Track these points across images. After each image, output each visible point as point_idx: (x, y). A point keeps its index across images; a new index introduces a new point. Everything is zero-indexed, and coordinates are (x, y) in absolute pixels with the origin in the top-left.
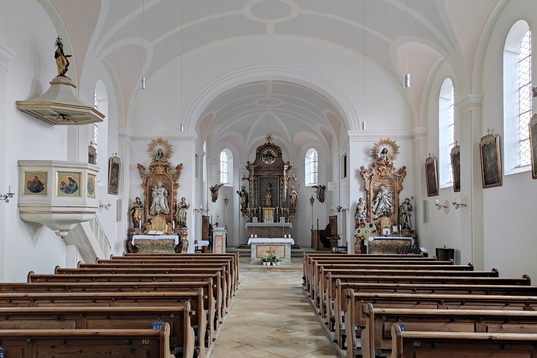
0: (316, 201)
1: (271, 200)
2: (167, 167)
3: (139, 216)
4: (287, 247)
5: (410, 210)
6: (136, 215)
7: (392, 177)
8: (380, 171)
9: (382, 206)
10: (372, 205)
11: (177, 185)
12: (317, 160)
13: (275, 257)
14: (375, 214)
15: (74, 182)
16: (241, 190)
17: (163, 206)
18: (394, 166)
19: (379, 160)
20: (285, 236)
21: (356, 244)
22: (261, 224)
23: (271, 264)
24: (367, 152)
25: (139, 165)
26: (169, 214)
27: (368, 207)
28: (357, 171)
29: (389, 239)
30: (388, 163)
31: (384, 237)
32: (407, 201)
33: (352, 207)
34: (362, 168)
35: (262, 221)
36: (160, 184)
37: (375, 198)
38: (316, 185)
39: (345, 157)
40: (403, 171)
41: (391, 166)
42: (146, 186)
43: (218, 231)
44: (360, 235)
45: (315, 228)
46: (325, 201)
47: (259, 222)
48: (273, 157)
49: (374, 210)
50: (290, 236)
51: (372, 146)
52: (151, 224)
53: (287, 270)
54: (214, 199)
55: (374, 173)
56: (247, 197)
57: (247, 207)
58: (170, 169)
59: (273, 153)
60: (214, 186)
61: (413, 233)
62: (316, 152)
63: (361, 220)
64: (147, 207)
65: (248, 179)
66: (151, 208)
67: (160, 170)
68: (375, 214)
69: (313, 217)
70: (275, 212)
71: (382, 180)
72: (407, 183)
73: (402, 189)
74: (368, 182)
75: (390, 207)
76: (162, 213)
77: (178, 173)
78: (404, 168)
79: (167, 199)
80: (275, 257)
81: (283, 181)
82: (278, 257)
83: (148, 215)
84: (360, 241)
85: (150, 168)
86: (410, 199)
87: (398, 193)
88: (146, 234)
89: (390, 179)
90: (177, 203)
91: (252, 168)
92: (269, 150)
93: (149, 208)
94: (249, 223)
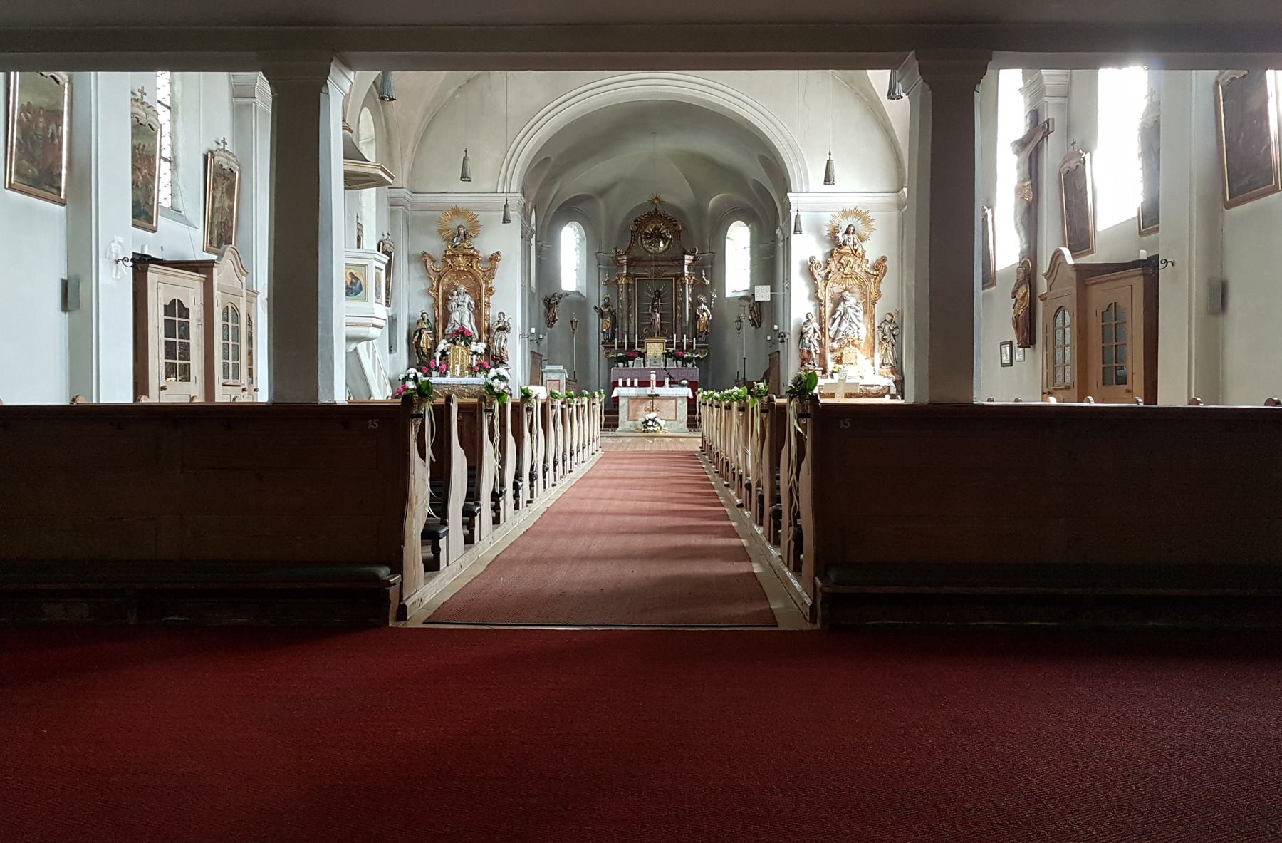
7: (863, 275)
10: (828, 323)
11: (490, 290)
34: (812, 259)
36: (463, 288)
37: (834, 313)
57: (613, 337)
63: (809, 352)
77: (493, 269)
78: (884, 259)
81: (683, 285)
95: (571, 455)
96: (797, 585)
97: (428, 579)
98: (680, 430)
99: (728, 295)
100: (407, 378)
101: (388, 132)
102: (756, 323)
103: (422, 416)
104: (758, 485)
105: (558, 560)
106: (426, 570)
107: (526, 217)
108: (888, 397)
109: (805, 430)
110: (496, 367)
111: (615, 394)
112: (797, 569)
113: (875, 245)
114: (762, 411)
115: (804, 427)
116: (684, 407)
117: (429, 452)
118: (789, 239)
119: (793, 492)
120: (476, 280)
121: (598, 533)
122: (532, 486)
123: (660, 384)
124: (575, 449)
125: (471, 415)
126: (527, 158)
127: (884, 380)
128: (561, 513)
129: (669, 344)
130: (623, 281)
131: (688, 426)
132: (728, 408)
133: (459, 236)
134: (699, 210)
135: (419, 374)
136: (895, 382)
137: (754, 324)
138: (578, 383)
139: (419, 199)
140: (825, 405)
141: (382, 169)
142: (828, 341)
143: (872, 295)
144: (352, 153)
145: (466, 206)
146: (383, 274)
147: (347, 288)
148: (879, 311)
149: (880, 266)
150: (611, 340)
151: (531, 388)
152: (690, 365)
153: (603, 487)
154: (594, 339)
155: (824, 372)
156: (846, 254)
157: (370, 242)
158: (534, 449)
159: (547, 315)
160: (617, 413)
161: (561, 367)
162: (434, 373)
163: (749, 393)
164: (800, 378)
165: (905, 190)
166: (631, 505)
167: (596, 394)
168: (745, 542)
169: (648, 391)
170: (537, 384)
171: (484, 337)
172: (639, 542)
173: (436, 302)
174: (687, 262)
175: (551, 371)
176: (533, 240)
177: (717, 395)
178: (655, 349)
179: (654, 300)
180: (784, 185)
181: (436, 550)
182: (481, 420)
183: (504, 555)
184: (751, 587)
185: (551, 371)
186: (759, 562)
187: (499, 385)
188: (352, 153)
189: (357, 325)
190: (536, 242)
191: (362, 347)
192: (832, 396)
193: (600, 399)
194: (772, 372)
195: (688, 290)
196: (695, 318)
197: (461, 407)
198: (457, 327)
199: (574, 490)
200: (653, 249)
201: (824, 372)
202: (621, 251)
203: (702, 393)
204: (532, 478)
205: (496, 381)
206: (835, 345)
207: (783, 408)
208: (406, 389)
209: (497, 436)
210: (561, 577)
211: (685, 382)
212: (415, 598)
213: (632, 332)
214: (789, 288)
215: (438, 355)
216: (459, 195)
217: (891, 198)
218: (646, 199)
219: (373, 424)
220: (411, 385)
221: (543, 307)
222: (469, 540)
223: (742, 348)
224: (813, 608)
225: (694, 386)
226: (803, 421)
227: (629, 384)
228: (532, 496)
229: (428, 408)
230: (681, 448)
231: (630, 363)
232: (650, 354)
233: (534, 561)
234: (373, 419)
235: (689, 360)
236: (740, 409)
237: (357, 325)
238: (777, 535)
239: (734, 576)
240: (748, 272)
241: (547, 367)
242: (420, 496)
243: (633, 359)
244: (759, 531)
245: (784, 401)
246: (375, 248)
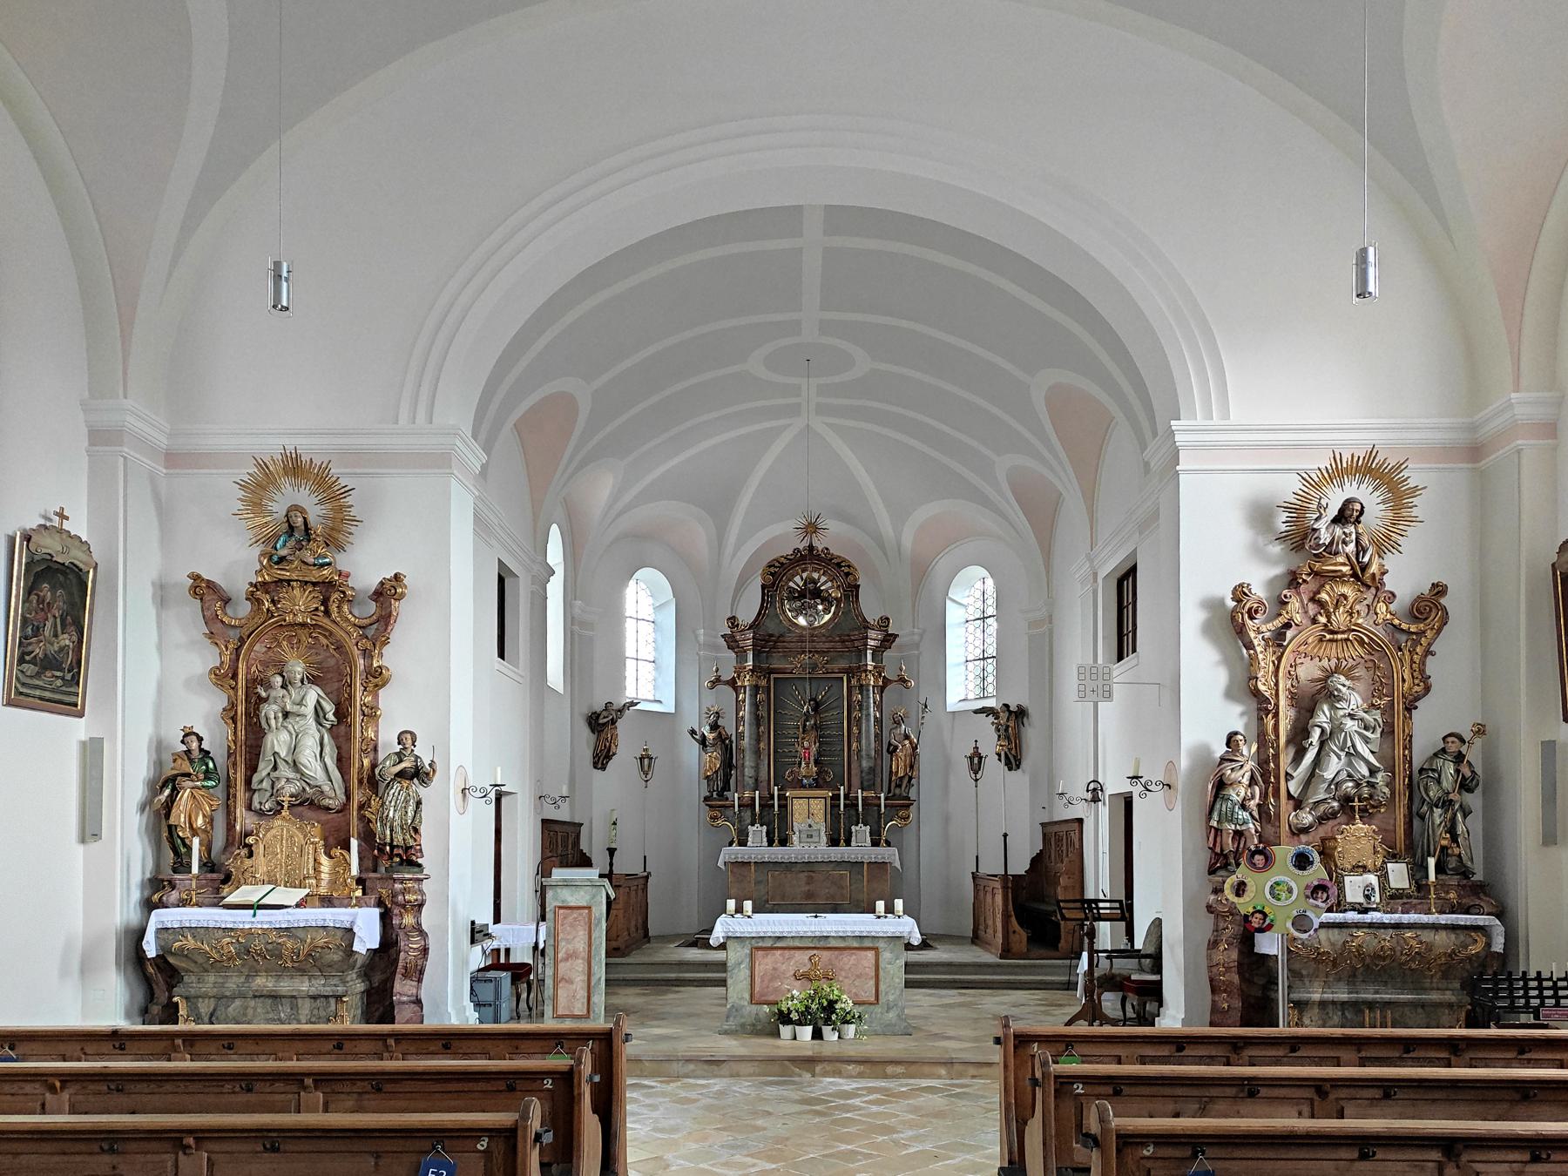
0: (993, 767)
1: (817, 763)
2: (329, 590)
3: (198, 818)
4: (886, 956)
5: (1466, 785)
6: (179, 817)
7: (1380, 632)
9: (1333, 766)
10: (1286, 759)
12: (991, 611)
13: (832, 1003)
14: (1298, 804)
17: (313, 768)
18: (1390, 583)
19: (1316, 553)
20: (880, 905)
21: (1213, 945)
22: (778, 853)
23: (817, 1035)
24: (1260, 515)
25: (196, 578)
26: (344, 808)
27: (1266, 773)
28: (1212, 605)
29: (1383, 926)
30: (1364, 568)
31: (1352, 916)
32: (1453, 747)
33: (1192, 770)
34: (1240, 593)
35: (784, 842)
36: (298, 669)
37: (1300, 734)
38: (991, 703)
39: (1127, 579)
40: (1429, 608)
41: (1376, 584)
42: (235, 676)
43: (567, 884)
44: (1245, 905)
45: (992, 865)
46: (1023, 765)
47: (770, 843)
48: (827, 601)
50: (899, 904)
51: (1288, 487)
52: (250, 855)
53: (890, 1069)
54: (602, 758)
55: (1298, 618)
57: (726, 787)
58: (345, 599)
59: (825, 584)
60: (599, 707)
61: (1481, 890)
62: (990, 582)
64: (240, 777)
65: (732, 683)
66: (256, 778)
67: (300, 603)
68: (1298, 804)
69: (977, 824)
70: (835, 806)
71: (1333, 650)
72: (1451, 661)
74: (1265, 659)
75: (1373, 771)
76: (307, 803)
77: (385, 619)
78: (1439, 590)
79: (335, 737)
80: (832, 1003)
81: (862, 688)
82: (846, 1003)
83: (240, 811)
84: (1231, 930)
85: (251, 597)
86: (1467, 736)
87: (1410, 708)
88: (217, 903)
89: (1371, 646)
90: (381, 757)
91: (748, 641)
92: (807, 572)
93: (248, 782)
94: (735, 847)
130: (747, 681)
156: (1337, 577)
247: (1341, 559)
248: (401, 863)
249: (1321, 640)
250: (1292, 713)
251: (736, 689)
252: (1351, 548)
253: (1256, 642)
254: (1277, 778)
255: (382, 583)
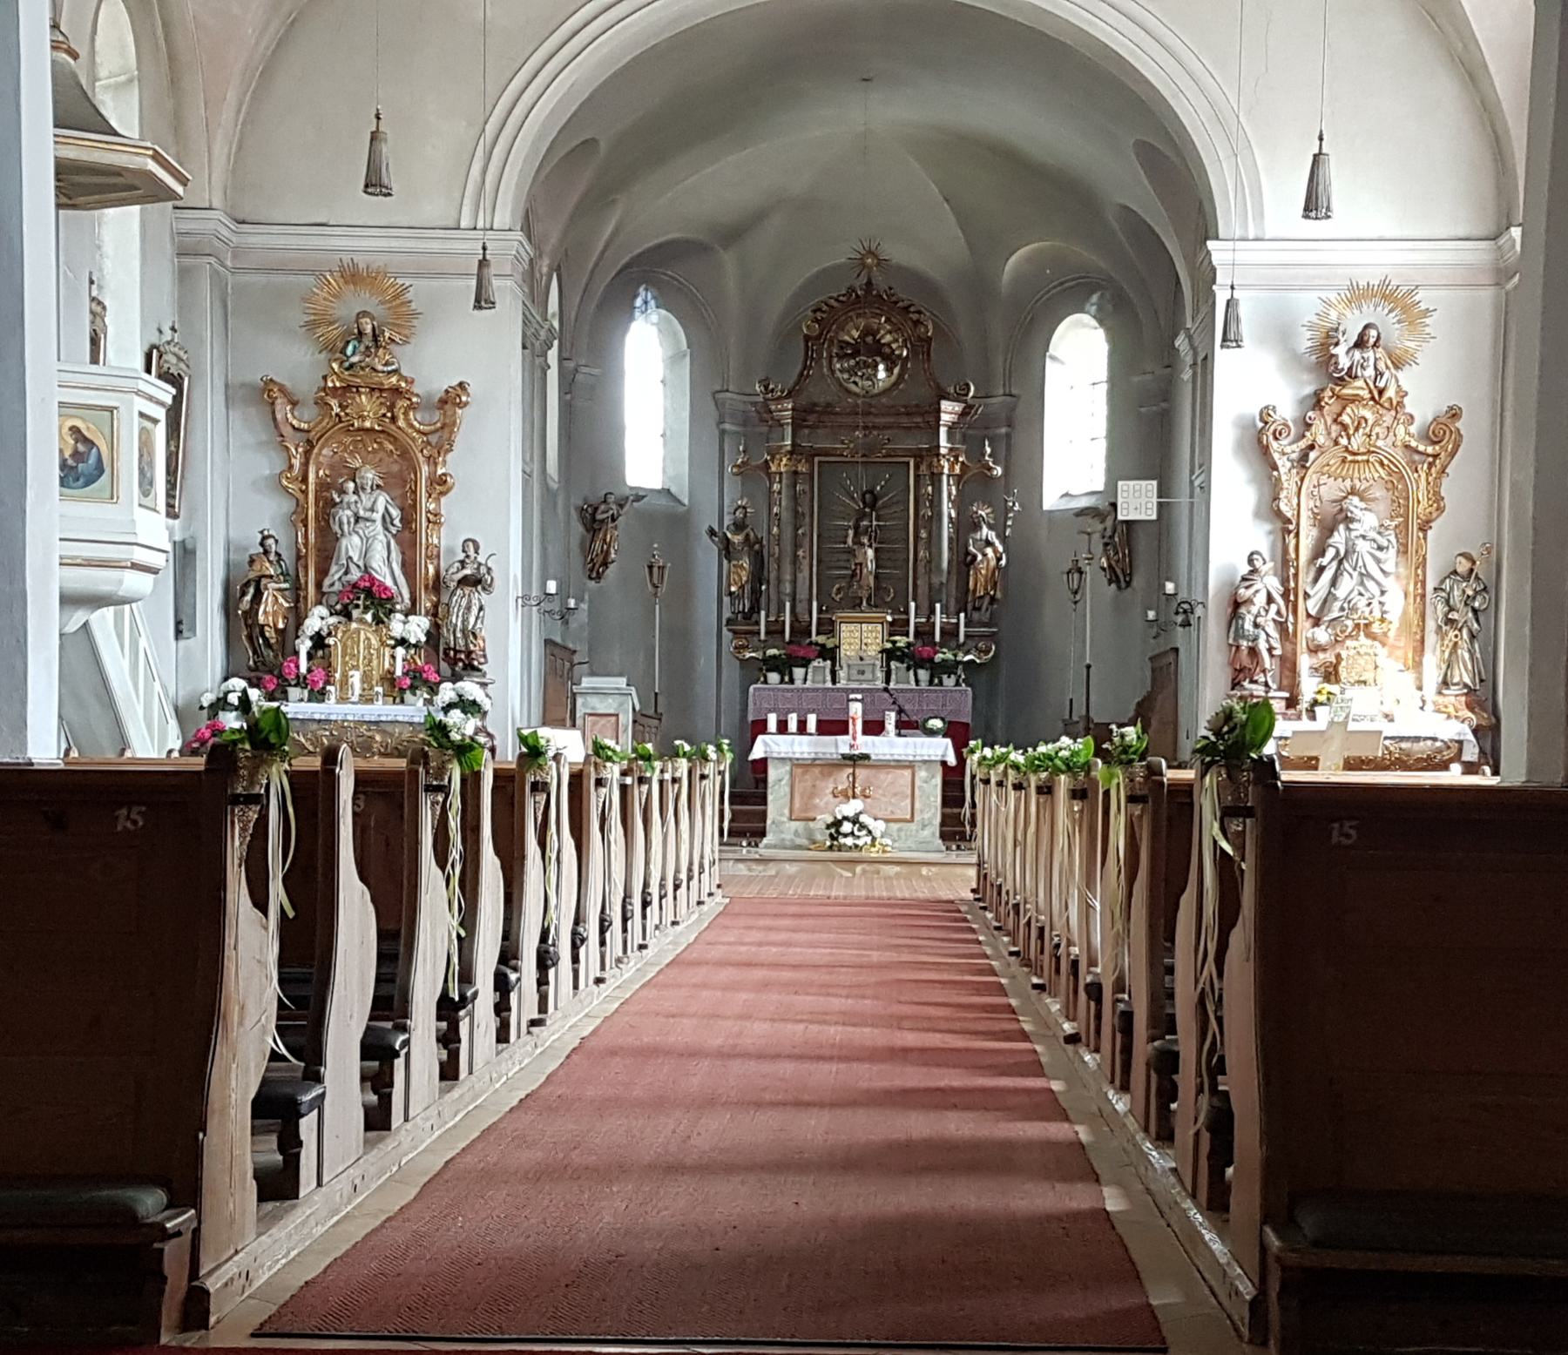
7: (1400, 456)
8: (1345, 427)
11: (442, 480)
14: (1317, 622)
15: (89, 443)
16: (727, 521)
18: (1410, 406)
30: (1381, 392)
34: (1266, 414)
36: (369, 476)
37: (1319, 552)
49: (1313, 606)
55: (1321, 440)
56: (759, 554)
57: (755, 609)
63: (1253, 652)
66: (327, 582)
68: (1317, 622)
73: (1441, 510)
77: (448, 427)
78: (1454, 414)
81: (936, 478)
95: (645, 904)
96: (1217, 1247)
97: (265, 1223)
98: (923, 846)
99: (1048, 504)
100: (221, 704)
101: (172, 58)
102: (1120, 576)
103: (260, 800)
104: (1120, 986)
105: (614, 1170)
106: (262, 1198)
107: (536, 296)
108: (1456, 768)
109: (1240, 848)
110: (455, 678)
111: (757, 753)
112: (1217, 1203)
113: (1433, 377)
114: (1132, 799)
115: (1238, 840)
116: (932, 788)
117: (277, 892)
118: (1208, 360)
119: (1208, 1005)
120: (405, 454)
121: (708, 1103)
122: (542, 982)
123: (874, 727)
124: (654, 890)
125: (389, 799)
126: (539, 137)
127: (1449, 725)
128: (613, 1052)
129: (899, 627)
130: (782, 465)
131: (943, 836)
132: (1046, 790)
133: (361, 341)
134: (979, 283)
135: (254, 694)
136: (1475, 731)
137: (1114, 579)
138: (664, 723)
139: (256, 238)
140: (1291, 787)
141: (157, 157)
142: (1304, 625)
143: (1423, 508)
144: (76, 111)
145: (379, 261)
146: (160, 432)
147: (63, 465)
148: (1439, 548)
149: (1443, 433)
150: (750, 615)
151: (544, 732)
152: (949, 682)
153: (726, 988)
154: (707, 610)
155: (1292, 702)
156: (1355, 399)
157: (126, 348)
158: (550, 887)
159: (586, 549)
160: (763, 800)
161: (622, 682)
162: (294, 692)
163: (1099, 752)
164: (1228, 715)
165: (1516, 232)
166: (796, 1032)
167: (711, 750)
168: (1084, 1133)
169: (842, 745)
170: (559, 723)
171: (426, 602)
172: (814, 1129)
173: (300, 508)
174: (945, 418)
175: (596, 692)
176: (553, 355)
177: (1017, 757)
178: (861, 639)
179: (862, 516)
180: (1200, 222)
181: (290, 1144)
182: (407, 810)
183: (469, 1158)
184: (1099, 1250)
185: (596, 692)
186: (1119, 1183)
187: (462, 725)
188: (76, 111)
189: (90, 563)
190: (561, 359)
191: (102, 621)
192: (1311, 763)
193: (719, 764)
194: (1157, 702)
195: (948, 489)
196: (964, 562)
197: (362, 780)
198: (355, 575)
199: (652, 993)
200: (859, 385)
201: (1292, 702)
202: (778, 387)
203: (979, 753)
204: (545, 961)
205: (456, 716)
206: (1322, 635)
207: (1184, 792)
208: (217, 731)
209: (455, 854)
210: (608, 1215)
211: (936, 723)
212: (230, 1270)
213: (802, 594)
214: (1206, 488)
215: (304, 646)
216: (361, 231)
217: (1479, 253)
218: (841, 254)
219: (128, 820)
220: (231, 721)
221: (578, 529)
222: (377, 1120)
223: (1083, 638)
224: (1258, 1306)
225: (958, 734)
226: (1235, 826)
227: (793, 725)
228: (543, 1008)
229: (276, 777)
230: (923, 892)
231: (798, 672)
232: (847, 651)
233: (542, 1175)
234: (130, 805)
235: (949, 668)
236: (1078, 794)
237: (90, 563)
238: (1165, 1115)
239: (1050, 1218)
240: (1101, 447)
241: (587, 682)
242: (251, 1008)
243: (805, 663)
244: (1121, 1104)
245: (1189, 775)
246: (139, 363)
247: (1360, 383)
248: (465, 668)
249: (1344, 461)
250: (1315, 532)
251: (769, 475)
252: (1370, 372)
253: (1279, 463)
254: (1296, 596)
255: (447, 391)
